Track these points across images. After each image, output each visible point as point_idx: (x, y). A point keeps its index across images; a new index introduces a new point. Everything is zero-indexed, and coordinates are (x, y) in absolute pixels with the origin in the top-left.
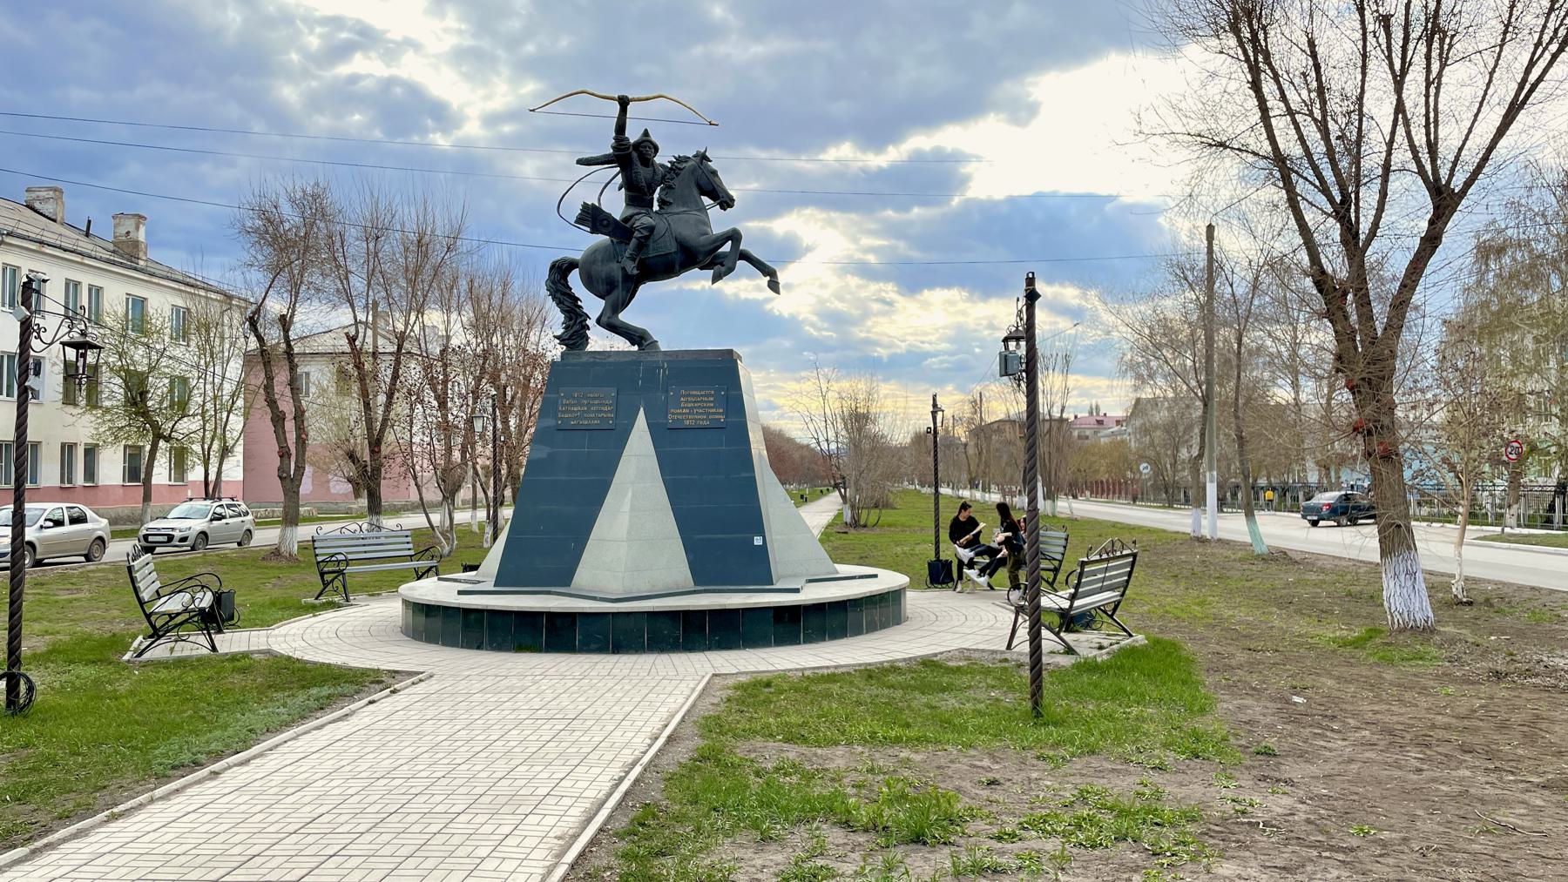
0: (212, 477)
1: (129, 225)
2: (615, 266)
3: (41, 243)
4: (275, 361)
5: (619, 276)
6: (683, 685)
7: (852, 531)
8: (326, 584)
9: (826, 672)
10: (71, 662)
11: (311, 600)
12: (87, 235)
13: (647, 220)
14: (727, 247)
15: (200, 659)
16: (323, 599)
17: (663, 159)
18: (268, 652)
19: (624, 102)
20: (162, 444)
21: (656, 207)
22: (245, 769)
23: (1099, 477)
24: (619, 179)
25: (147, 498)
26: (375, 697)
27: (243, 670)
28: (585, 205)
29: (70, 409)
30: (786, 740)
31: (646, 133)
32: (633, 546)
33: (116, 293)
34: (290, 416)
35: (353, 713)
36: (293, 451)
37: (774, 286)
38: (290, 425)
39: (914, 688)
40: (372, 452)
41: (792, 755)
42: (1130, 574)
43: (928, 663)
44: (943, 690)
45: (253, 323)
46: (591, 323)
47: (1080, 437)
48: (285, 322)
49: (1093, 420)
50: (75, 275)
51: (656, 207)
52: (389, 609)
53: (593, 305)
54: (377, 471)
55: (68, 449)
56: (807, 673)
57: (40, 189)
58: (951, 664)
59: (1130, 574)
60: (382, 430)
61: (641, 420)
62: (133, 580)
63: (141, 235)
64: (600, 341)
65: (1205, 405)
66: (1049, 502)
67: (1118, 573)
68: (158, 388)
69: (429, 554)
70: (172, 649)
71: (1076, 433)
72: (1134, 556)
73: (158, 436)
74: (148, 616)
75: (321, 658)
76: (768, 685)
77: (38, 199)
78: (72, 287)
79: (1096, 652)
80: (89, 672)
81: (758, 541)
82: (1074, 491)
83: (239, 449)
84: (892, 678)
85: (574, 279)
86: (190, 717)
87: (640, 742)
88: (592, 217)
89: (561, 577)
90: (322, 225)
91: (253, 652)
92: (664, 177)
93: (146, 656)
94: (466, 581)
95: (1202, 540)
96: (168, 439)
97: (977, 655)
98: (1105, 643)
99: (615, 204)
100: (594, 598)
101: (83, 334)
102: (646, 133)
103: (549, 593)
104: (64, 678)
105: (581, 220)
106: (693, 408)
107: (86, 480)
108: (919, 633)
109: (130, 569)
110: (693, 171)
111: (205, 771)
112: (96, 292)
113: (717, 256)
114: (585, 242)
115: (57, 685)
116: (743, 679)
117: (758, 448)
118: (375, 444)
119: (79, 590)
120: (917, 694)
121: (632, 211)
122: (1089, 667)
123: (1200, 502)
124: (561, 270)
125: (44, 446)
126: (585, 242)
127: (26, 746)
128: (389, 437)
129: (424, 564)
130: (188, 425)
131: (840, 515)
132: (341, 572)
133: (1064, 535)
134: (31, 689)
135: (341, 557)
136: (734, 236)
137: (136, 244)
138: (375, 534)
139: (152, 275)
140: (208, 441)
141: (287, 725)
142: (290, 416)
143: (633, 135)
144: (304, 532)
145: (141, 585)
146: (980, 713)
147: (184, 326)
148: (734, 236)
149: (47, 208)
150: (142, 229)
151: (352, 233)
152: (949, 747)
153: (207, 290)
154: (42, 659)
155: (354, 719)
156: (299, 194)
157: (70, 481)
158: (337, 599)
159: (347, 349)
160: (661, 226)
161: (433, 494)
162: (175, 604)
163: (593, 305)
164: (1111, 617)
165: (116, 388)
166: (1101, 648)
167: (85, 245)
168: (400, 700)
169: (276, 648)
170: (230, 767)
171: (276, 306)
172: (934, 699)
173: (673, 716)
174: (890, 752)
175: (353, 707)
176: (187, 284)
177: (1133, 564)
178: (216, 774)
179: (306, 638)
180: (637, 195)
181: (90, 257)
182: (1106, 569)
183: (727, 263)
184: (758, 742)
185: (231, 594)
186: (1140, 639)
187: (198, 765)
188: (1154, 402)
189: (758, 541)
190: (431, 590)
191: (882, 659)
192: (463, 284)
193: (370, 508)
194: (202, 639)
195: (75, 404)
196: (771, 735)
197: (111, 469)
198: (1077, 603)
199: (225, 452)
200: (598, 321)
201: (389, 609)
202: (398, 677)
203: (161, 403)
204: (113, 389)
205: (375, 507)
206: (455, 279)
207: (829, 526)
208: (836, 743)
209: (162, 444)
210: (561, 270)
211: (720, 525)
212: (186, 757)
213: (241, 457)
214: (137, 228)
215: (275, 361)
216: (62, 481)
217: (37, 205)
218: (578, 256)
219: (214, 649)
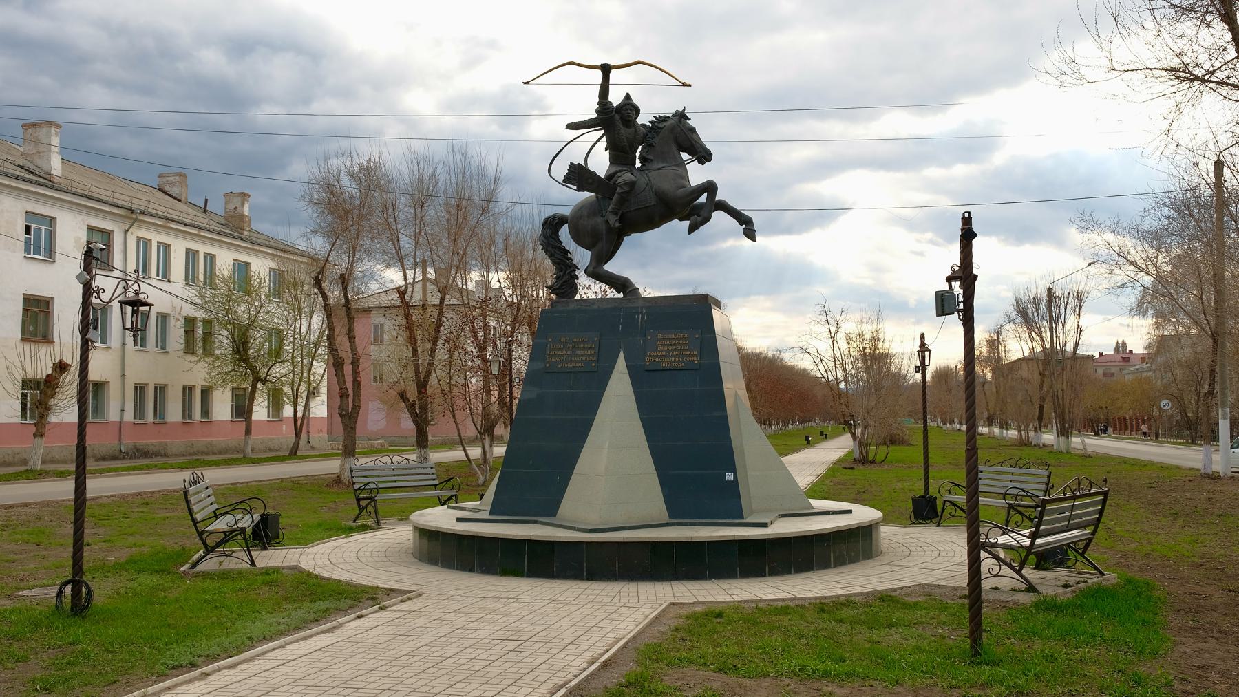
0: (300, 414)
1: (236, 202)
2: (599, 220)
3: (167, 219)
4: (345, 314)
5: (603, 228)
6: (640, 612)
7: (861, 467)
8: (361, 509)
9: (780, 604)
10: (140, 571)
11: (350, 523)
12: (205, 212)
13: (628, 177)
14: (703, 199)
15: (240, 572)
16: (359, 522)
17: (644, 119)
18: (297, 569)
20: (259, 386)
21: (638, 164)
22: (232, 671)
23: (1121, 414)
24: (603, 143)
25: (248, 431)
26: (364, 612)
27: (271, 584)
29: (189, 357)
30: (719, 670)
31: (628, 97)
32: (613, 477)
33: (225, 259)
34: (348, 362)
35: (341, 625)
36: (351, 392)
37: (750, 234)
38: (348, 369)
39: (861, 623)
40: (420, 392)
41: (716, 685)
42: (1101, 512)
43: (885, 598)
44: (890, 626)
45: (318, 282)
47: (1105, 375)
48: (344, 281)
49: (1118, 358)
50: (194, 245)
51: (638, 164)
52: (400, 535)
53: (581, 256)
54: (424, 408)
55: (188, 390)
56: (761, 605)
57: (168, 175)
58: (909, 599)
59: (1101, 512)
60: (428, 375)
62: (188, 502)
63: (246, 211)
64: (588, 288)
65: (1215, 341)
66: (1062, 439)
67: (1087, 509)
68: (257, 339)
69: (452, 485)
70: (221, 563)
71: (1100, 371)
72: (1106, 494)
73: (257, 379)
74: (200, 534)
75: (336, 575)
76: (720, 615)
77: (168, 183)
78: (191, 255)
79: (1060, 590)
80: (148, 580)
81: (729, 477)
82: (1098, 429)
83: (324, 390)
84: (844, 613)
85: (564, 233)
86: (213, 623)
87: (582, 661)
89: (548, 508)
90: (376, 194)
91: (283, 568)
92: (645, 136)
93: (200, 567)
94: (470, 510)
95: (1213, 477)
96: (264, 382)
97: (937, 591)
98: (1073, 581)
99: (600, 163)
100: (572, 528)
101: (137, 293)
102: (628, 97)
103: (535, 522)
104: (130, 584)
105: (568, 179)
106: (668, 350)
107: (202, 416)
108: (887, 568)
109: (186, 493)
110: (672, 129)
111: (196, 673)
112: (210, 258)
113: (696, 207)
114: (572, 198)
115: (122, 591)
116: (697, 609)
117: (734, 387)
118: (422, 385)
119: (175, 510)
120: (864, 629)
122: (1050, 606)
123: (1212, 437)
125: (170, 388)
126: (572, 198)
127: (73, 644)
128: (433, 380)
129: (446, 493)
130: (280, 370)
131: (850, 453)
132: (372, 499)
133: (1046, 473)
134: (89, 594)
135: (373, 486)
136: (710, 188)
137: (242, 217)
138: (424, 465)
139: (254, 243)
140: (296, 385)
141: (282, 634)
142: (348, 362)
143: (615, 98)
144: (363, 461)
145: (195, 508)
146: (919, 650)
147: (281, 284)
148: (710, 188)
149: (175, 191)
150: (247, 205)
151: (402, 202)
152: (876, 683)
153: (295, 253)
154: (103, 569)
155: (339, 632)
156: (356, 169)
157: (190, 417)
158: (370, 522)
159: (399, 303)
160: (642, 181)
161: (470, 431)
162: (222, 524)
163: (581, 256)
164: (1082, 554)
165: (224, 340)
166: (1066, 586)
167: (202, 220)
168: (386, 615)
169: (304, 565)
170: (219, 670)
171: (339, 263)
172: (876, 635)
173: (617, 642)
174: (815, 686)
175: (342, 620)
176: (282, 250)
177: (1104, 502)
178: (206, 675)
179: (332, 557)
180: (620, 153)
181: (205, 230)
182: (1072, 508)
183: (704, 213)
184: (690, 671)
185: (276, 517)
186: (1111, 577)
187: (194, 666)
188: (1177, 338)
189: (729, 477)
190: (441, 518)
191: (840, 592)
192: (499, 242)
193: (418, 442)
194: (243, 555)
195: (193, 353)
196: (705, 664)
197: (222, 407)
198: (1038, 541)
199: (312, 393)
201: (400, 535)
202: (392, 595)
203: (259, 351)
204: (223, 340)
205: (422, 441)
206: (492, 238)
207: (840, 461)
208: (765, 675)
209: (259, 386)
210: (552, 225)
211: (694, 461)
212: (185, 660)
213: (324, 397)
214: (243, 205)
215: (345, 314)
216: (184, 417)
217: (167, 189)
218: (567, 211)
219: (253, 564)
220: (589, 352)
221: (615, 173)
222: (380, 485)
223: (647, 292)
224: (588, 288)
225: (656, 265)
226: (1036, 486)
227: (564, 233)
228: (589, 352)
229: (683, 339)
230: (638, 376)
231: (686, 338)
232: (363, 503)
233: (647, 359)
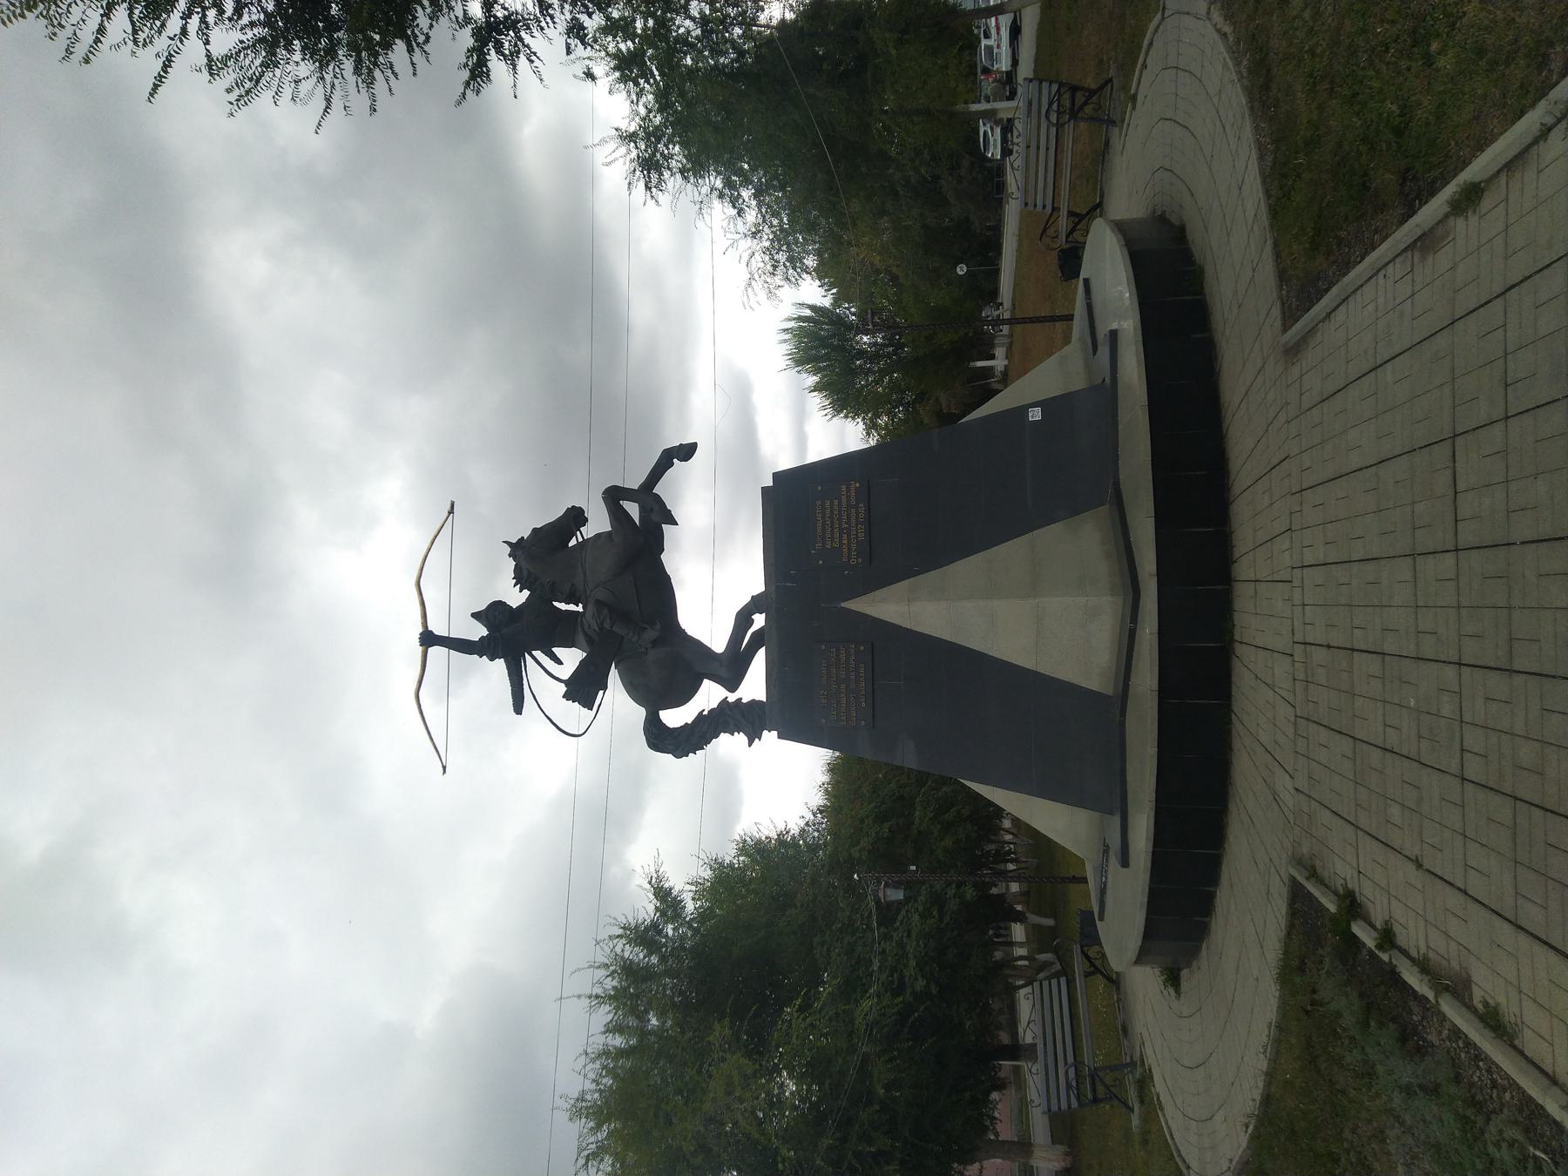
14: (633, 509)
19: (429, 639)
28: (567, 696)
31: (475, 616)
37: (687, 452)
46: (732, 698)
53: (710, 695)
61: (859, 605)
81: (1035, 414)
85: (674, 718)
88: (583, 689)
99: (571, 658)
102: (475, 616)
105: (588, 703)
114: (616, 699)
121: (581, 638)
124: (660, 738)
126: (616, 699)
143: (478, 632)
148: (614, 496)
163: (710, 695)
189: (1035, 414)
200: (732, 689)
220: (843, 657)
221: (585, 634)
222: (1070, 1059)
223: (759, 587)
224: (754, 686)
225: (716, 579)
226: (1045, 92)
227: (674, 718)
228: (843, 657)
229: (823, 509)
230: (877, 578)
231: (823, 505)
232: (1101, 1091)
233: (853, 562)
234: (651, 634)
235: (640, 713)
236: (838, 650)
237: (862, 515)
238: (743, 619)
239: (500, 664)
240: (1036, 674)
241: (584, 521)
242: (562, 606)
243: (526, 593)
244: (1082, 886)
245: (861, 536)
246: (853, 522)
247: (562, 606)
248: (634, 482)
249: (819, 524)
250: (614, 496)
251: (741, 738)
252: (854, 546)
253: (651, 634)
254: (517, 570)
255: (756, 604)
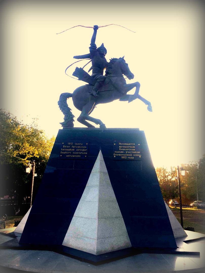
19: (96, 28)
31: (103, 45)
46: (75, 119)
53: (76, 113)
61: (100, 156)
85: (70, 102)
88: (80, 73)
102: (103, 45)
105: (75, 74)
143: (98, 45)
220: (83, 150)
224: (77, 125)
225: (110, 115)
233: (114, 154)
234: (94, 93)
235: (72, 92)
236: (85, 149)
237: (130, 158)
238: (97, 122)
239: (88, 52)
240: (73, 216)
241: (130, 79)
242: (105, 70)
243: (108, 61)
244: (3, 227)
245: (123, 157)
246: (127, 155)
247: (105, 70)
248: (140, 93)
249: (127, 144)
250: (137, 85)
251: (63, 121)
252: (120, 155)
253: (94, 93)
254: (116, 59)
255: (102, 126)
